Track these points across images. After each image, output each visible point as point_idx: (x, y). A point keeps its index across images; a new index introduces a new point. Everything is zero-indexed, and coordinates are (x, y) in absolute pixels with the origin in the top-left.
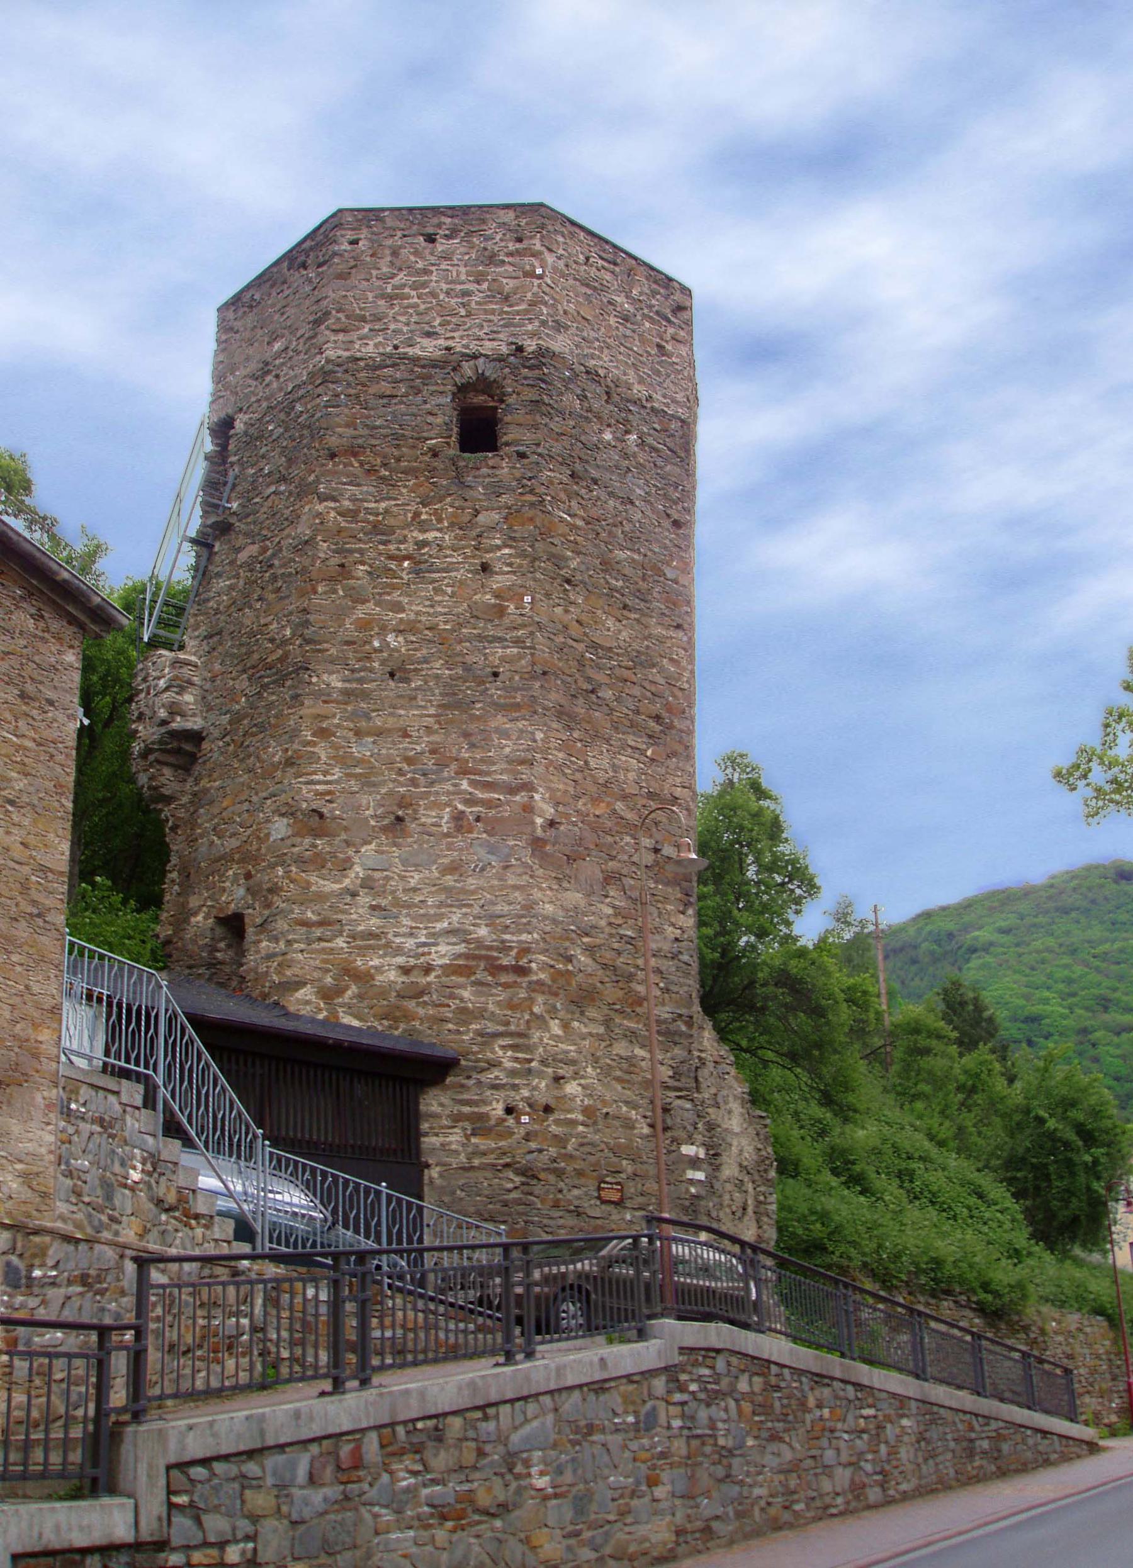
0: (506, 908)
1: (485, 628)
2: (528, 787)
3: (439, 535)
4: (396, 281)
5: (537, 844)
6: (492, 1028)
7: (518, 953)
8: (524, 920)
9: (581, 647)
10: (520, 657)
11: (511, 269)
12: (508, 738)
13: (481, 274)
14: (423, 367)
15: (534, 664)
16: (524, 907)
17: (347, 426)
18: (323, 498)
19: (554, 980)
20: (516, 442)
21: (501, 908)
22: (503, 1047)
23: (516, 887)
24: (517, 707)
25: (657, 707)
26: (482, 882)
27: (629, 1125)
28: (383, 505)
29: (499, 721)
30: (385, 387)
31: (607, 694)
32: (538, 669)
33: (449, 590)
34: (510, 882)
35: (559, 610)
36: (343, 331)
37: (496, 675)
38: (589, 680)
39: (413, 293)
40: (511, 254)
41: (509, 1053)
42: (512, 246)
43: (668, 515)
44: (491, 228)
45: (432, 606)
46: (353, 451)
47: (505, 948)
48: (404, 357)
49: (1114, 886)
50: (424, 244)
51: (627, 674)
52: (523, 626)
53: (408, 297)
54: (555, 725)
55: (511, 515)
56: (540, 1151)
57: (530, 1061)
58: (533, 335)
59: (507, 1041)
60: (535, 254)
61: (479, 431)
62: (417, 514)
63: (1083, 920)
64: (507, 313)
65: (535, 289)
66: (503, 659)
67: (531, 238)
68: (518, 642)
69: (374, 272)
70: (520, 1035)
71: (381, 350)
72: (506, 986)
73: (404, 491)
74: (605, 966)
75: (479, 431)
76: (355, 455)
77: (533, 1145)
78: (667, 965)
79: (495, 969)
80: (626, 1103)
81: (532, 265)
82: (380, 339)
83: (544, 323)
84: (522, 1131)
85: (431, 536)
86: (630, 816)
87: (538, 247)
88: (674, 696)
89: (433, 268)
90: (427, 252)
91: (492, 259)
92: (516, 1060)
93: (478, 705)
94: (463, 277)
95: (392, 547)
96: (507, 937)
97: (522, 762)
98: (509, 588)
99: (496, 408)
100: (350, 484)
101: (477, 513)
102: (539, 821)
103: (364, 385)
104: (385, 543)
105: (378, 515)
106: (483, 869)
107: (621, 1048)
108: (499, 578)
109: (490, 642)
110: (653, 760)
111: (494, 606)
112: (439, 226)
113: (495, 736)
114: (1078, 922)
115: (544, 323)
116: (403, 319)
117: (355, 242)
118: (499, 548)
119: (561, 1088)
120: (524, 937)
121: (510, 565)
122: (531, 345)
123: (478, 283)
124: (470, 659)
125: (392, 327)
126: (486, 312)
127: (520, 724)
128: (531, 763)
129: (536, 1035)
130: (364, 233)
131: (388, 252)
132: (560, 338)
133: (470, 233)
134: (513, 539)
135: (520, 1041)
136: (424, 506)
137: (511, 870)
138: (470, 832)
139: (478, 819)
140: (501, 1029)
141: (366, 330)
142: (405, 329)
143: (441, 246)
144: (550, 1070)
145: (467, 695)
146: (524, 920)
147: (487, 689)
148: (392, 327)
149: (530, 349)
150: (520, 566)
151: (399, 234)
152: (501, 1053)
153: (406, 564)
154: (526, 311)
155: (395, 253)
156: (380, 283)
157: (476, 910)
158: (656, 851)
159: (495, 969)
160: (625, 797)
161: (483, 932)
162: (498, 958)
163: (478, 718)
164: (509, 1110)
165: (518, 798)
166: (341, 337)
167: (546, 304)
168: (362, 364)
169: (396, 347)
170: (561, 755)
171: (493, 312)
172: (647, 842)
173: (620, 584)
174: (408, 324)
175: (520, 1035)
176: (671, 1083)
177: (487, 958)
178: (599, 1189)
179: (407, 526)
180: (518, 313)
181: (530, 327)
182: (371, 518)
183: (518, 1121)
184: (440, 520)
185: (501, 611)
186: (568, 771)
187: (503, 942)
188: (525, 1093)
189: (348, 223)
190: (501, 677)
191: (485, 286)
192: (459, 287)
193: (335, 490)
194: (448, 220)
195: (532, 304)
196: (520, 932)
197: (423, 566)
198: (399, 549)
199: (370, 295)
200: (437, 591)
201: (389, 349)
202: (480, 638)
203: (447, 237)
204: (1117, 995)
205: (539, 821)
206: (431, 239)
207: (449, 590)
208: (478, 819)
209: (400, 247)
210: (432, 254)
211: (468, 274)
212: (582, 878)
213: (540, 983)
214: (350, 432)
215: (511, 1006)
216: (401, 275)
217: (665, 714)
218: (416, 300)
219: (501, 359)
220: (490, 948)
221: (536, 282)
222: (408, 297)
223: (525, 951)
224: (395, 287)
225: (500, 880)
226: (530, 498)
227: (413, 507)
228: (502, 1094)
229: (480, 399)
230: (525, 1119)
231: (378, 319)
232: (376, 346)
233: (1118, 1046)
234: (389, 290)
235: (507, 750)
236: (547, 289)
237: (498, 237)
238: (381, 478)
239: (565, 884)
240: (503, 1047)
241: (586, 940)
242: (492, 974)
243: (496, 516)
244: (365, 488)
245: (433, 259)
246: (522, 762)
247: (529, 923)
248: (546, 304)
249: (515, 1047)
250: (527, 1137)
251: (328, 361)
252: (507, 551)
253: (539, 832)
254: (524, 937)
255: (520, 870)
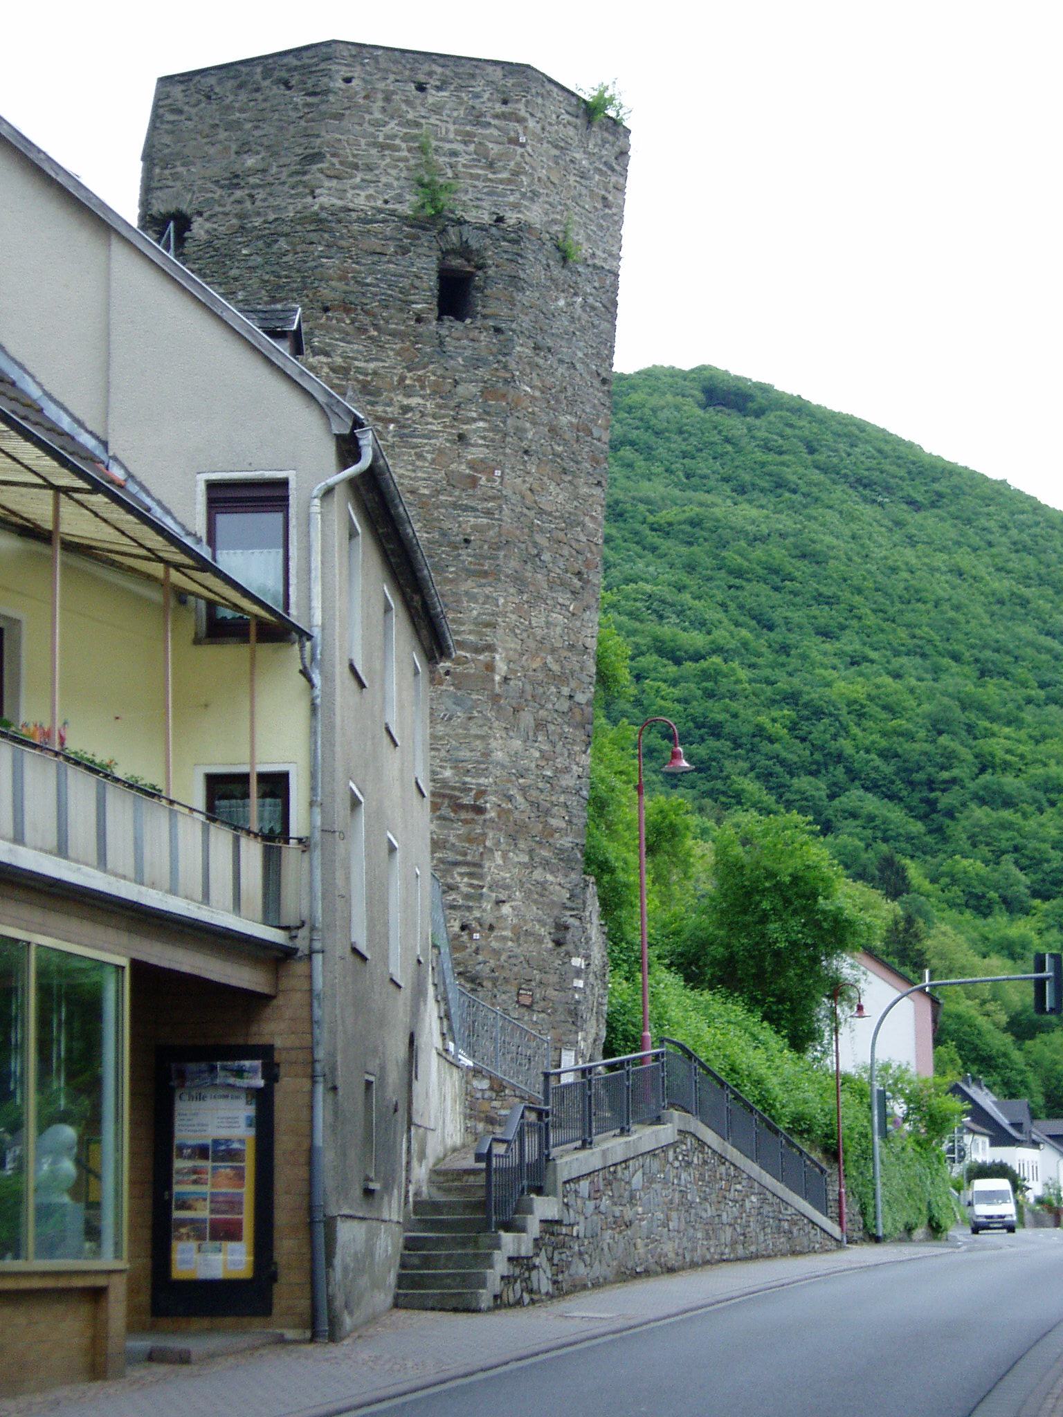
0: (469, 754)
1: (460, 498)
2: (490, 648)
3: (421, 401)
4: (386, 129)
5: (495, 698)
6: (451, 856)
7: (476, 794)
8: (483, 766)
9: (531, 514)
10: (490, 527)
11: (496, 133)
12: (476, 602)
13: (468, 134)
14: (412, 226)
15: (500, 535)
16: (484, 755)
17: (340, 279)
18: (316, 352)
19: (499, 817)
20: (494, 316)
21: (464, 754)
22: (461, 874)
23: (477, 737)
24: (485, 574)
25: (578, 565)
26: (448, 730)
27: (540, 940)
28: (372, 365)
29: (468, 585)
30: (375, 244)
31: (546, 557)
32: (503, 539)
33: (429, 457)
34: (472, 732)
35: (519, 481)
36: (336, 177)
37: (467, 541)
38: (535, 545)
39: (404, 145)
40: (496, 116)
41: (466, 880)
42: (499, 108)
43: (599, 375)
44: (479, 85)
45: (414, 471)
46: (347, 308)
47: (465, 789)
48: (393, 213)
49: (700, 412)
50: (415, 92)
51: (561, 535)
52: (493, 498)
53: (398, 149)
54: (512, 590)
55: (488, 391)
56: (485, 963)
57: (482, 887)
58: (516, 207)
59: (464, 869)
60: (521, 120)
61: (455, 295)
62: (402, 379)
63: (640, 464)
64: (491, 180)
65: (518, 158)
66: (475, 528)
67: (518, 101)
68: (488, 513)
69: (367, 117)
70: (475, 865)
71: (373, 204)
72: (465, 822)
73: (391, 353)
74: (532, 803)
75: (455, 295)
76: (347, 311)
77: (480, 958)
78: (573, 801)
79: (457, 807)
80: (539, 921)
81: (516, 132)
82: (371, 191)
83: (523, 195)
84: (474, 947)
85: (414, 401)
86: (556, 668)
87: (523, 113)
88: (591, 552)
89: (423, 121)
90: (418, 102)
91: (477, 119)
92: (471, 885)
93: (452, 569)
94: (451, 136)
95: (380, 408)
96: (468, 779)
97: (487, 625)
98: (482, 461)
99: (472, 274)
100: (342, 340)
101: (456, 383)
102: (497, 678)
103: (356, 239)
104: (373, 404)
105: (367, 375)
106: (450, 719)
107: (538, 874)
108: (473, 450)
109: (465, 510)
110: (573, 614)
111: (469, 476)
112: (430, 74)
113: (465, 599)
114: (630, 466)
115: (523, 195)
116: (393, 172)
117: (348, 80)
118: (474, 420)
119: (499, 910)
120: (482, 780)
121: (484, 438)
122: (512, 218)
123: (465, 143)
124: (446, 525)
125: (384, 179)
126: (472, 176)
127: (488, 590)
128: (493, 625)
129: (487, 864)
130: (357, 72)
131: (380, 96)
132: (535, 207)
133: (460, 88)
134: (488, 413)
135: (472, 870)
136: (410, 371)
137: (475, 721)
138: (441, 684)
139: (447, 673)
140: (460, 858)
141: (358, 180)
142: (395, 183)
143: (433, 97)
144: (494, 895)
145: (441, 559)
146: (483, 766)
147: (460, 555)
148: (384, 179)
149: (512, 222)
150: (493, 440)
151: (392, 77)
152: (458, 879)
153: (392, 427)
154: (509, 181)
155: (387, 99)
156: (371, 129)
157: (443, 754)
158: (571, 697)
159: (457, 807)
160: (553, 651)
161: (448, 773)
162: (459, 798)
163: (451, 581)
164: (463, 928)
165: (481, 657)
166: (334, 183)
167: (525, 173)
168: (354, 215)
169: (386, 202)
170: (514, 617)
171: (477, 177)
172: (566, 691)
173: (560, 449)
174: (398, 179)
175: (475, 865)
176: (569, 904)
177: (451, 797)
178: (518, 994)
179: (394, 389)
180: (501, 181)
181: (511, 199)
182: (361, 377)
183: (471, 938)
184: (423, 388)
185: (474, 482)
186: (518, 631)
187: (465, 783)
188: (477, 914)
189: (343, 58)
190: (472, 545)
191: (472, 148)
192: (448, 146)
193: (329, 345)
194: (439, 70)
195: (516, 173)
196: (480, 776)
197: (406, 431)
198: (385, 412)
199: (363, 141)
200: (420, 456)
201: (379, 203)
202: (455, 506)
203: (439, 88)
204: (686, 597)
205: (497, 678)
206: (421, 88)
207: (429, 457)
208: (447, 673)
209: (394, 93)
210: (423, 105)
211: (457, 133)
212: (522, 726)
213: (492, 820)
214: (340, 285)
215: (470, 840)
216: (392, 124)
217: (584, 570)
218: (405, 153)
219: (482, 228)
220: (454, 788)
221: (520, 150)
222: (398, 149)
223: (481, 793)
224: (387, 137)
225: (465, 729)
226: (502, 373)
227: (399, 371)
228: (458, 914)
229: (456, 262)
230: (476, 936)
231: (369, 168)
232: (369, 197)
233: (674, 683)
234: (381, 139)
235: (475, 612)
236: (528, 159)
237: (486, 95)
238: (370, 338)
239: (511, 734)
240: (461, 874)
241: (521, 781)
242: (455, 812)
243: (473, 389)
244: (356, 347)
245: (423, 112)
246: (487, 625)
247: (486, 769)
248: (525, 173)
249: (471, 875)
250: (477, 951)
251: (322, 208)
252: (481, 424)
253: (497, 690)
254: (482, 780)
255: (480, 722)
